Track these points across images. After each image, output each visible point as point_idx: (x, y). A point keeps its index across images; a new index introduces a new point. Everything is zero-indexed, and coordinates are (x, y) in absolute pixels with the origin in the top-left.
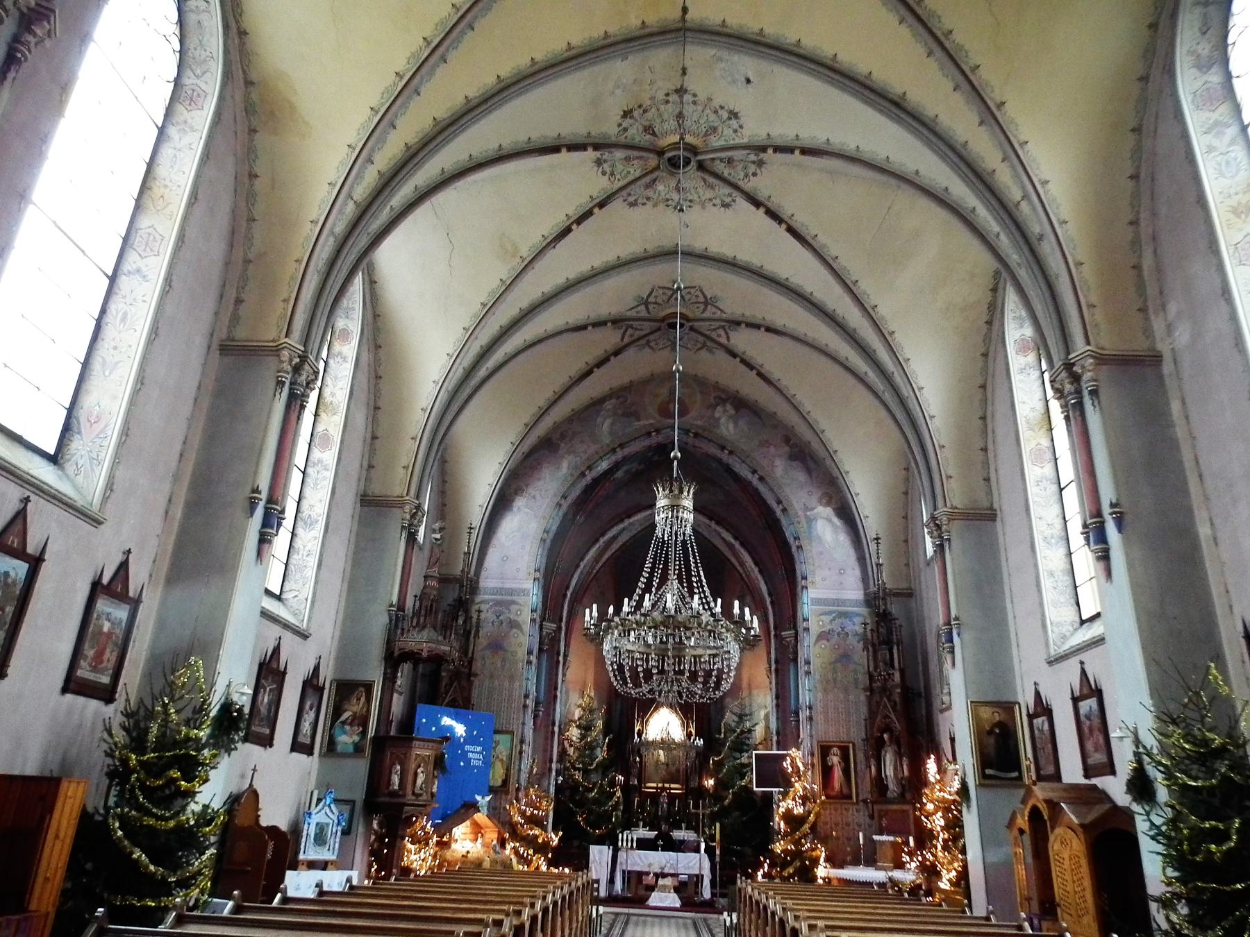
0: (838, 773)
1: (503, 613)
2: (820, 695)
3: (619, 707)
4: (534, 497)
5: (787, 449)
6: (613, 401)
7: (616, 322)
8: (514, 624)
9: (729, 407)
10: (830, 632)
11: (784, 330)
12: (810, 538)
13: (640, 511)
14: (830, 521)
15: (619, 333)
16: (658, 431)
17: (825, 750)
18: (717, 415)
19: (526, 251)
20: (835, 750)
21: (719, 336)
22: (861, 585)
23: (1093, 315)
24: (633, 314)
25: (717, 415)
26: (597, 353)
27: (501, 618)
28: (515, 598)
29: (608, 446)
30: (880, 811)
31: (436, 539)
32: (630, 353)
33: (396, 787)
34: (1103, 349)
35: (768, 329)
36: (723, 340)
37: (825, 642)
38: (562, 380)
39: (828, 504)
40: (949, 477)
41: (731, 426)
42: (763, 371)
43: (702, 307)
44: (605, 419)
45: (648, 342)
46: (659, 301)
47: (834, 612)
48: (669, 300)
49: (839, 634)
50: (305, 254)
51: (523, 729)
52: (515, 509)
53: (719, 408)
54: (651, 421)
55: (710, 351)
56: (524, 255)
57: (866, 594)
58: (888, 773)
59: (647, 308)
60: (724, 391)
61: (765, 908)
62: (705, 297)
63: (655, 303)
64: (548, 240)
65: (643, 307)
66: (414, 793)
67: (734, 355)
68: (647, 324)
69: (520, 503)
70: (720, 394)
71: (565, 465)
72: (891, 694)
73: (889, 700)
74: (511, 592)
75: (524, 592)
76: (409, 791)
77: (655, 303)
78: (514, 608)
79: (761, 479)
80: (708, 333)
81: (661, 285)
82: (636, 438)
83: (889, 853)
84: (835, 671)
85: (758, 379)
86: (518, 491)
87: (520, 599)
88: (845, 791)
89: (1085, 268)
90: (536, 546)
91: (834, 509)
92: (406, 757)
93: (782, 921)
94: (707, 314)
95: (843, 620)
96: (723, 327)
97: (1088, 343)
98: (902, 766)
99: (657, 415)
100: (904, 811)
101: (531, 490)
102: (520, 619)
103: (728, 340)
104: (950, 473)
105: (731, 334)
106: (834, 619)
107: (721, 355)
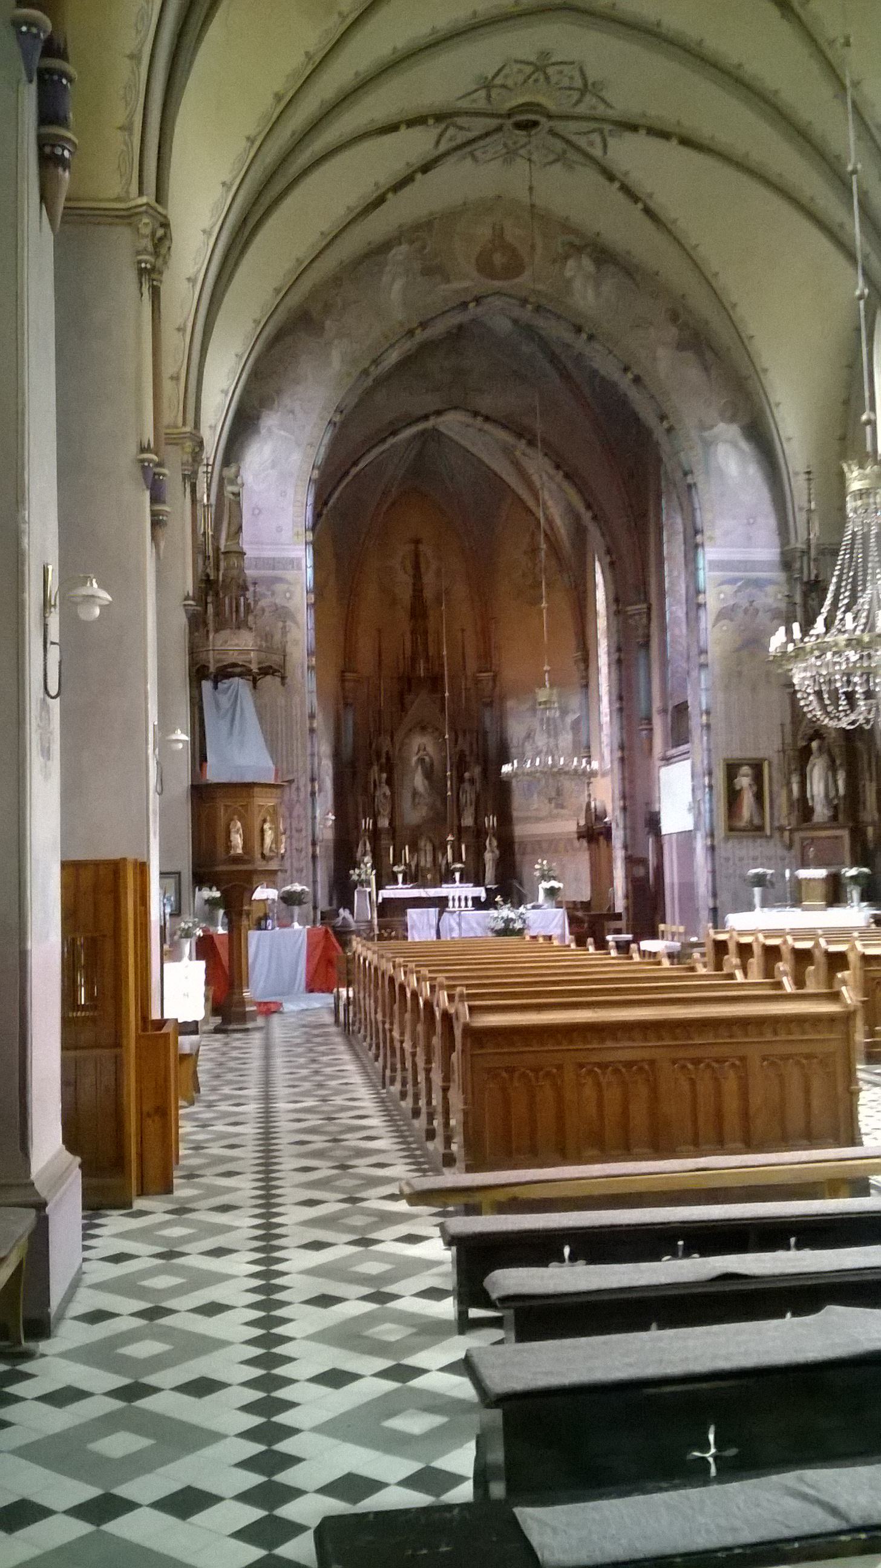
0: (748, 800)
2: (721, 696)
3: (350, 723)
4: (292, 412)
5: (674, 331)
6: (404, 248)
7: (441, 117)
10: (734, 608)
12: (707, 473)
14: (735, 445)
17: (732, 770)
18: (568, 274)
20: (745, 769)
22: (776, 540)
24: (464, 104)
25: (568, 274)
26: (397, 168)
28: (278, 573)
29: (401, 324)
30: (803, 839)
33: (240, 851)
35: (686, 142)
36: (597, 152)
37: (726, 622)
39: (732, 420)
41: (590, 293)
42: (652, 205)
43: (576, 95)
44: (394, 280)
46: (510, 82)
47: (741, 579)
48: (525, 81)
50: (143, 43)
52: (263, 431)
53: (571, 263)
54: (466, 284)
55: (570, 167)
56: (345, 9)
57: (782, 553)
58: (815, 792)
60: (575, 232)
61: (402, 987)
63: (503, 86)
65: (482, 93)
66: (263, 856)
67: (611, 177)
69: (270, 421)
70: (571, 238)
71: (336, 356)
75: (293, 563)
77: (503, 86)
78: (279, 587)
82: (444, 313)
83: (820, 889)
87: (289, 575)
88: (756, 821)
91: (743, 428)
92: (246, 811)
93: (428, 1005)
94: (582, 109)
96: (601, 131)
98: (835, 781)
99: (475, 274)
100: (837, 837)
101: (286, 401)
102: (290, 605)
103: (605, 152)
105: (611, 142)
106: (739, 590)
107: (590, 177)
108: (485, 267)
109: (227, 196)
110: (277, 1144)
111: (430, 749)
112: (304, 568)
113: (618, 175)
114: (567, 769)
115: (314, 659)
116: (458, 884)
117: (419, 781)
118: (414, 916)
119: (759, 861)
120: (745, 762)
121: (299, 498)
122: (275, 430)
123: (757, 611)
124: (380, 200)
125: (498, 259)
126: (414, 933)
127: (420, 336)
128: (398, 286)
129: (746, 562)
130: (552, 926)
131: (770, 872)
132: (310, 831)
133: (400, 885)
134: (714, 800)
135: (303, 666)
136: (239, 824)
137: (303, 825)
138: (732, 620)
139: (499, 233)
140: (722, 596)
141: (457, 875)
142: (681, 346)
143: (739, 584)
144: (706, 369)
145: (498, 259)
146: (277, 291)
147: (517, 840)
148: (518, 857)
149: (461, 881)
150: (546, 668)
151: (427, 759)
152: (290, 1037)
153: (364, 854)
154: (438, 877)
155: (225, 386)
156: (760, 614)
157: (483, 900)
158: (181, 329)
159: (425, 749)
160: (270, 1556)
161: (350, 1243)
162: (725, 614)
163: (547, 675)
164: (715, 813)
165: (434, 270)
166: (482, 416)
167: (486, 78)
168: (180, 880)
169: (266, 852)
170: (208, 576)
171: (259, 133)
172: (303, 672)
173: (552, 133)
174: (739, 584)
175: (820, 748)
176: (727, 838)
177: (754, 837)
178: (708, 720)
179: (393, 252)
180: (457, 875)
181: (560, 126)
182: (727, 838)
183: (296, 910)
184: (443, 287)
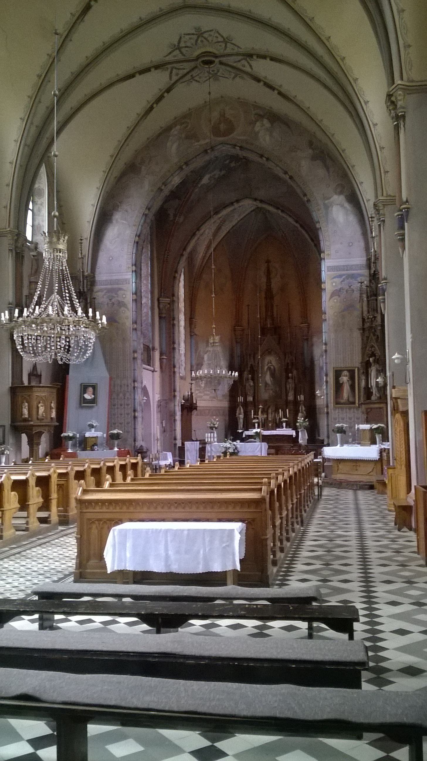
0: (346, 388)
1: (113, 297)
2: (333, 336)
5: (310, 151)
6: (178, 127)
8: (121, 304)
9: (265, 121)
11: (281, 58)
13: (225, 207)
14: (342, 206)
15: (167, 73)
16: (212, 149)
18: (257, 129)
19: (61, 28)
20: (346, 373)
21: (244, 66)
22: (364, 254)
23: (408, 54)
26: (150, 96)
27: (113, 300)
28: (120, 286)
31: (33, 256)
32: (180, 88)
33: (27, 416)
34: (413, 81)
35: (272, 59)
36: (248, 69)
37: (336, 297)
38: (133, 117)
39: (341, 193)
40: (386, 172)
41: (268, 138)
42: (282, 90)
45: (192, 77)
46: (189, 44)
47: (344, 275)
49: (347, 291)
51: (134, 373)
52: (114, 221)
53: (258, 124)
54: (207, 141)
55: (242, 78)
58: (372, 385)
59: (181, 53)
60: (259, 108)
62: (222, 37)
64: (77, 16)
65: (177, 52)
66: (38, 419)
67: (258, 80)
68: (185, 64)
69: (117, 216)
72: (375, 331)
73: (374, 335)
74: (117, 282)
75: (126, 281)
76: (35, 417)
77: (186, 47)
78: (120, 293)
79: (291, 178)
80: (235, 64)
81: (186, 32)
83: (368, 435)
84: (343, 317)
85: (279, 98)
86: (115, 208)
87: (124, 287)
88: (351, 399)
89: (406, 15)
90: (131, 247)
94: (228, 51)
95: (350, 280)
97: (402, 79)
100: (380, 408)
103: (252, 69)
104: (388, 168)
108: (216, 131)
109: (23, 123)
110: (358, 552)
111: (274, 363)
112: (131, 283)
113: (261, 78)
114: (221, 375)
115: (323, 318)
116: (284, 428)
117: (268, 378)
118: (188, 446)
119: (337, 421)
120: (345, 369)
121: (129, 251)
122: (119, 220)
123: (353, 291)
124: (151, 108)
125: (222, 127)
126: (188, 453)
127: (187, 170)
128: (175, 146)
129: (347, 266)
130: (256, 451)
131: (345, 425)
132: (133, 405)
133: (284, 428)
134: (329, 387)
135: (130, 329)
136: (26, 404)
137: (129, 402)
138: (339, 296)
139: (223, 114)
140: (334, 284)
141: (284, 424)
142: (314, 158)
143: (344, 277)
144: (328, 169)
145: (222, 127)
146: (112, 156)
147: (317, 407)
148: (318, 415)
149: (286, 427)
150: (214, 326)
151: (272, 367)
152: (368, 500)
153: (240, 414)
154: (275, 425)
155: (93, 202)
156: (355, 292)
157: (294, 436)
158: (8, 185)
159: (271, 363)
160: (212, 746)
161: (411, 604)
162: (336, 293)
163: (214, 329)
164: (329, 395)
165: (192, 136)
166: (235, 202)
167: (175, 45)
168: (4, 429)
169: (40, 417)
170: (80, 290)
171: (33, 94)
172: (130, 331)
173: (221, 63)
174: (344, 277)
175: (374, 361)
176: (335, 408)
177: (350, 408)
178: (326, 348)
179: (173, 130)
180: (284, 424)
181: (224, 59)
182: (335, 408)
183: (116, 442)
184: (196, 144)
